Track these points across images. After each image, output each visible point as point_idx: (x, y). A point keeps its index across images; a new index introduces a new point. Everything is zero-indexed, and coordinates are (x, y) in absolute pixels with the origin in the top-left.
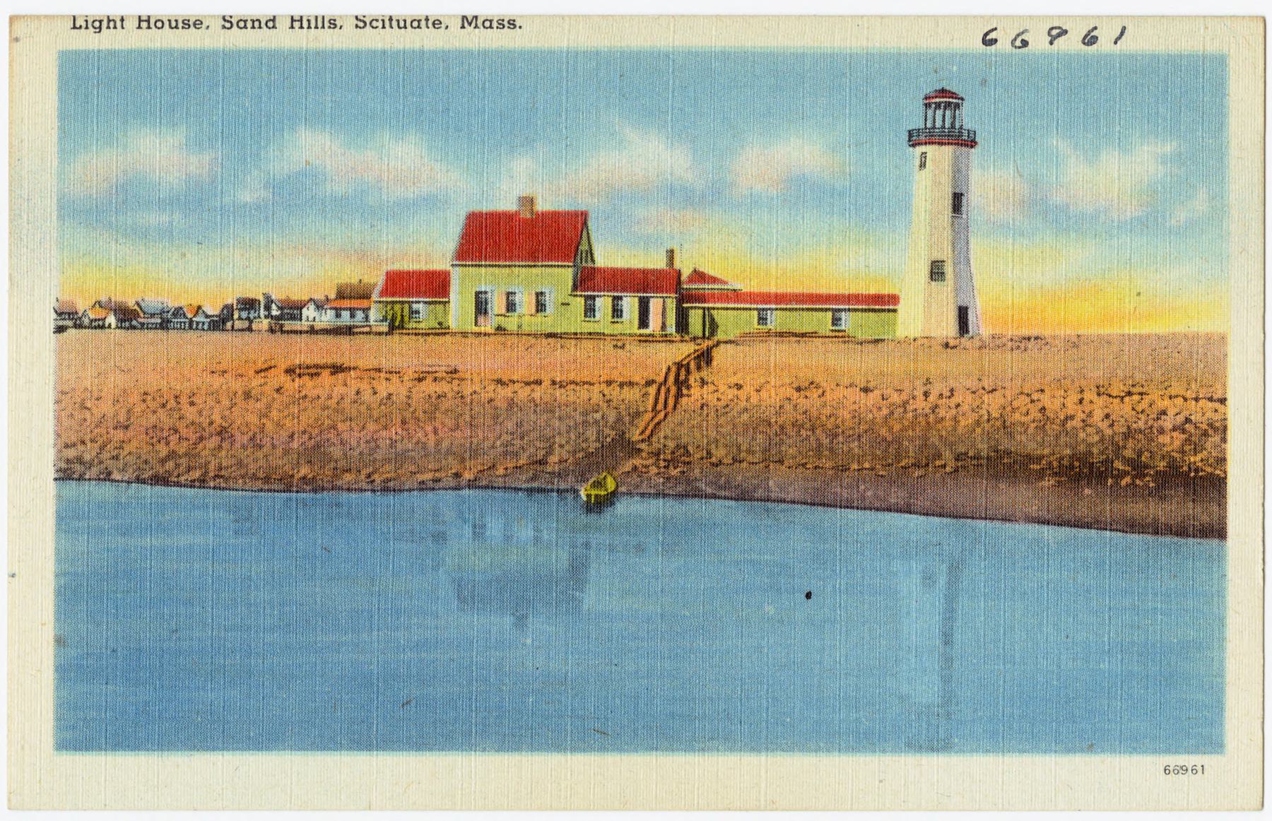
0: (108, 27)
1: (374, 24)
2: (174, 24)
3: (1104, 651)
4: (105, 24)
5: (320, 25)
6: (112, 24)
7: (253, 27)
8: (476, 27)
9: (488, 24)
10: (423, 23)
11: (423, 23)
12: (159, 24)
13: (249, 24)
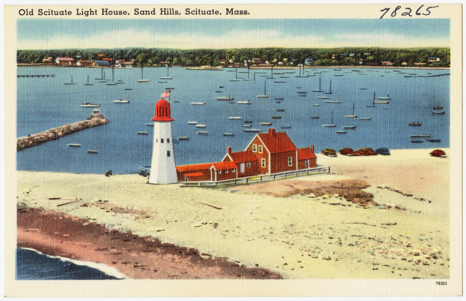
0: (91, 14)
1: (46, 13)
2: (116, 13)
3: (137, 263)
4: (89, 13)
5: (172, 13)
6: (92, 13)
7: (146, 14)
8: (232, 14)
9: (237, 13)
10: (212, 12)
11: (212, 12)
12: (236, 12)
13: (145, 13)
